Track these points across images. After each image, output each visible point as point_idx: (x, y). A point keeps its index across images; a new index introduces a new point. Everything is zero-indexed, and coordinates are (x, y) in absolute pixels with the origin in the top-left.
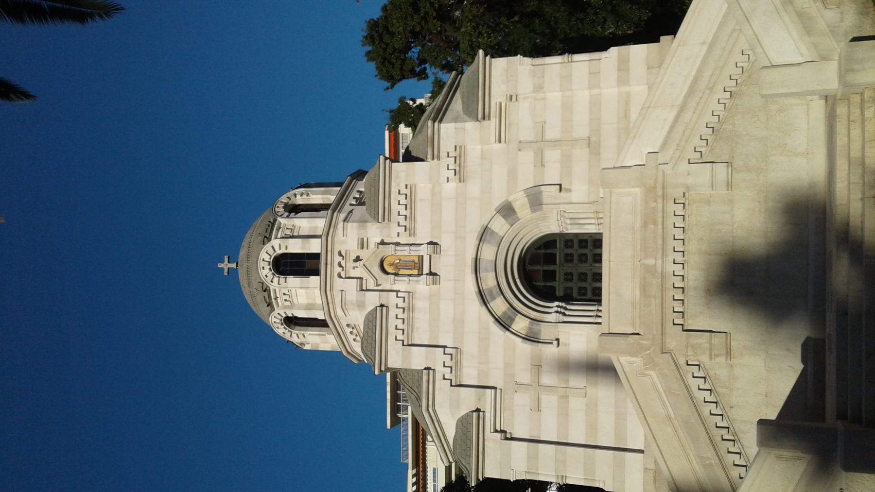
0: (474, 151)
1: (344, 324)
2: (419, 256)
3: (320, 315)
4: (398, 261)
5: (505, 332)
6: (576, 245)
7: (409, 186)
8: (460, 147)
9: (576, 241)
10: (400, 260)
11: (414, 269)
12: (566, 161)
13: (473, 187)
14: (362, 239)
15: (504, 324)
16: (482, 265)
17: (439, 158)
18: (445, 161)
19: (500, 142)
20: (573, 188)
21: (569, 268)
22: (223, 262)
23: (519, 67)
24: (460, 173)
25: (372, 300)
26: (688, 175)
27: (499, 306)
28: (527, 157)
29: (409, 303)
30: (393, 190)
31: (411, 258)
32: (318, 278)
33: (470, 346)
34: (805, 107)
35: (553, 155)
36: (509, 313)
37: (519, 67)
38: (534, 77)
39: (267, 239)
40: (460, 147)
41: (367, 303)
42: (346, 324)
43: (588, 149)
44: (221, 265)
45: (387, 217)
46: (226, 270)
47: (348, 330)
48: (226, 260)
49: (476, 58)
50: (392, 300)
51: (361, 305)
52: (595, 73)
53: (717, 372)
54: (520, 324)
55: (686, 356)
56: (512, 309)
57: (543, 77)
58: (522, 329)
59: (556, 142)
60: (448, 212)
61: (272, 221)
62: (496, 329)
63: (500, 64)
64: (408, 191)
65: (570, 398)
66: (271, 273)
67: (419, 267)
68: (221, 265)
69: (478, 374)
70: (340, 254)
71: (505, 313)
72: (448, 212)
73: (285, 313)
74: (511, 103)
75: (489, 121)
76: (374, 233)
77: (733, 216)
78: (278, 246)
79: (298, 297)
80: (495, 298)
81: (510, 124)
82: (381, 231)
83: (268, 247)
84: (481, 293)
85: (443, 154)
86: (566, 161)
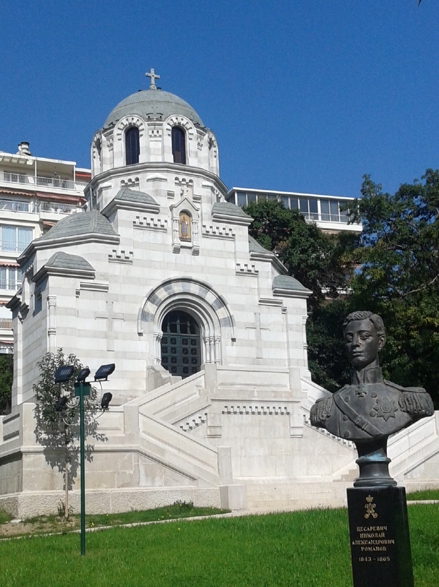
0: (250, 282)
1: (139, 176)
2: (190, 239)
3: (142, 158)
4: (187, 224)
5: (146, 296)
6: (192, 347)
7: (233, 237)
8: (257, 275)
9: (196, 347)
10: (187, 225)
11: (182, 235)
12: (249, 343)
13: (233, 281)
14: (200, 199)
15: (151, 297)
16: (186, 284)
17: (251, 260)
18: (250, 263)
19: (260, 301)
20: (234, 347)
21: (179, 340)
22: (155, 73)
23: (301, 316)
24: (241, 273)
25: (164, 202)
26: (298, 415)
27: (162, 294)
28: (250, 318)
29: (160, 229)
30: (232, 225)
31: (189, 233)
32: (172, 161)
33: (134, 271)
34: (328, 473)
35: (252, 334)
36: (158, 300)
37: (301, 316)
38: (296, 325)
39: (197, 125)
40: (257, 275)
41: (160, 198)
42: (139, 177)
43: (256, 357)
44: (153, 71)
45: (217, 219)
46: (149, 75)
47: (133, 178)
48: (157, 76)
49: (307, 289)
50: (162, 217)
51: (157, 192)
52: (298, 363)
53: (201, 430)
54: (151, 308)
55: (210, 413)
56: (160, 303)
57: (296, 331)
58: (148, 309)
59: (259, 337)
60: (218, 262)
61: (205, 129)
62: (148, 290)
63: (303, 304)
64: (230, 236)
65: (106, 339)
66: (177, 123)
67: (183, 239)
68: (153, 71)
69: (116, 276)
70: (191, 181)
71: (157, 297)
72: (218, 262)
73: (143, 130)
74: (281, 310)
75: (272, 295)
76: (206, 208)
77: (278, 438)
78: (192, 132)
79: (155, 142)
80: (166, 291)
81: (269, 308)
82: (206, 213)
83: (190, 125)
84: (169, 282)
85: (253, 263)
86: (249, 343)
